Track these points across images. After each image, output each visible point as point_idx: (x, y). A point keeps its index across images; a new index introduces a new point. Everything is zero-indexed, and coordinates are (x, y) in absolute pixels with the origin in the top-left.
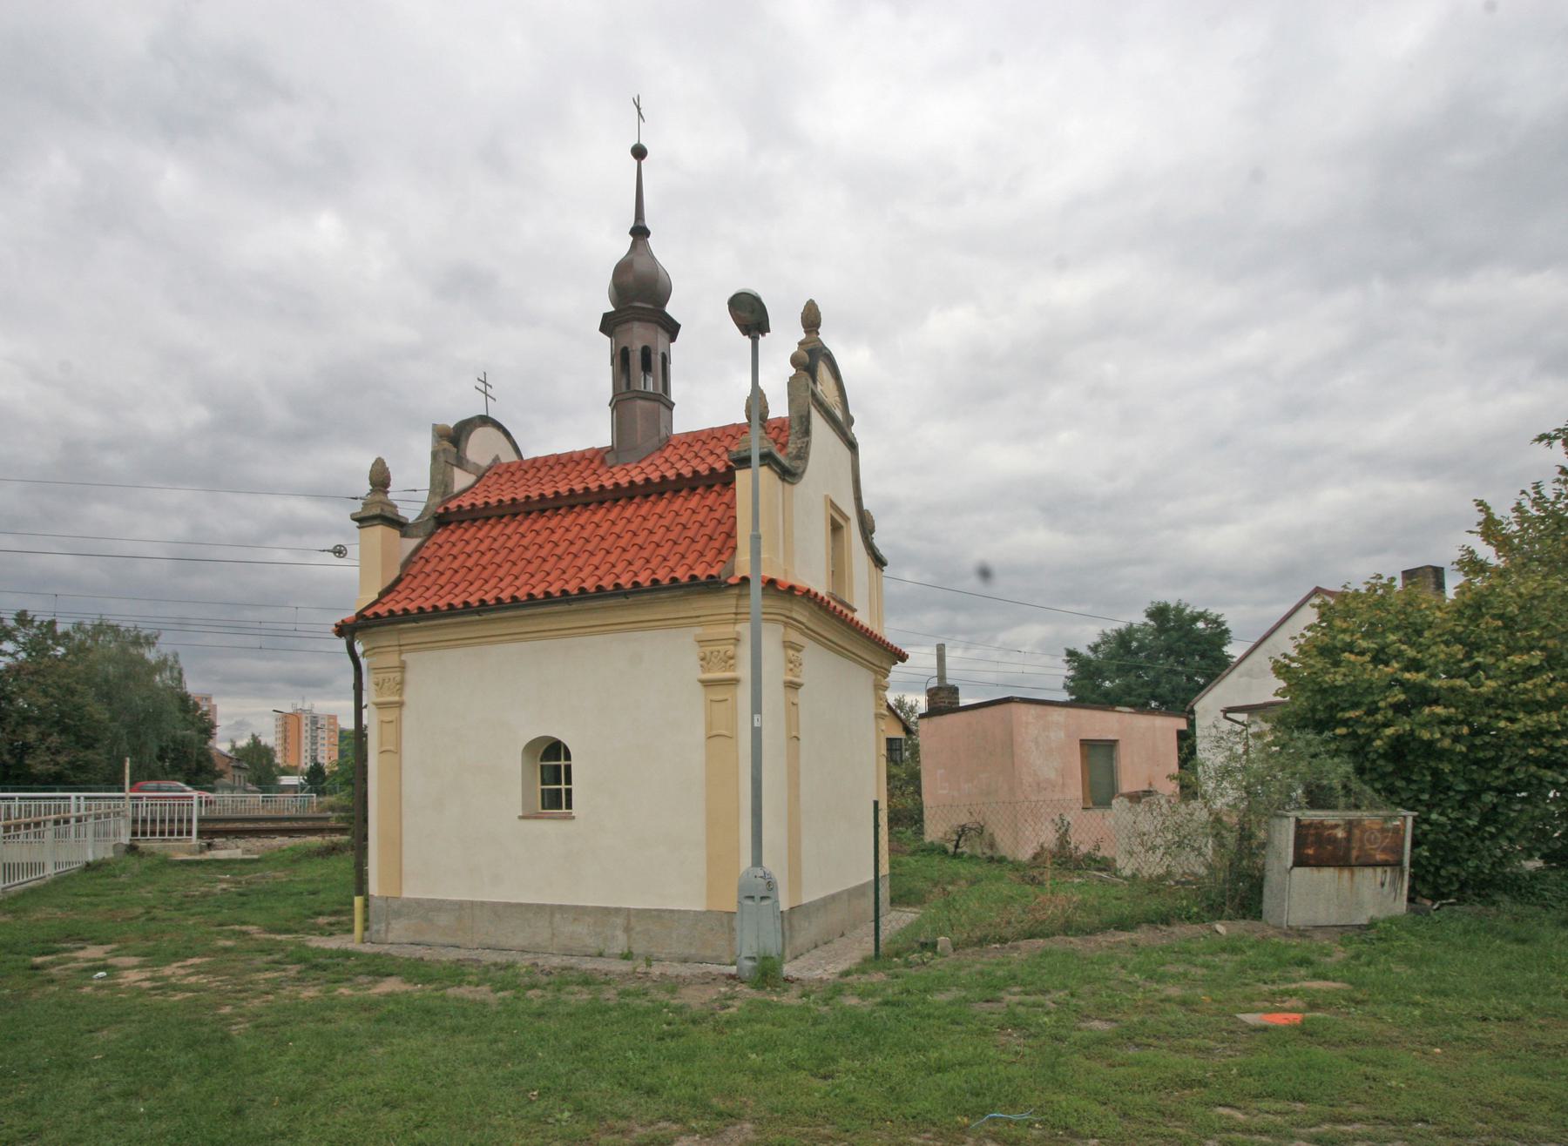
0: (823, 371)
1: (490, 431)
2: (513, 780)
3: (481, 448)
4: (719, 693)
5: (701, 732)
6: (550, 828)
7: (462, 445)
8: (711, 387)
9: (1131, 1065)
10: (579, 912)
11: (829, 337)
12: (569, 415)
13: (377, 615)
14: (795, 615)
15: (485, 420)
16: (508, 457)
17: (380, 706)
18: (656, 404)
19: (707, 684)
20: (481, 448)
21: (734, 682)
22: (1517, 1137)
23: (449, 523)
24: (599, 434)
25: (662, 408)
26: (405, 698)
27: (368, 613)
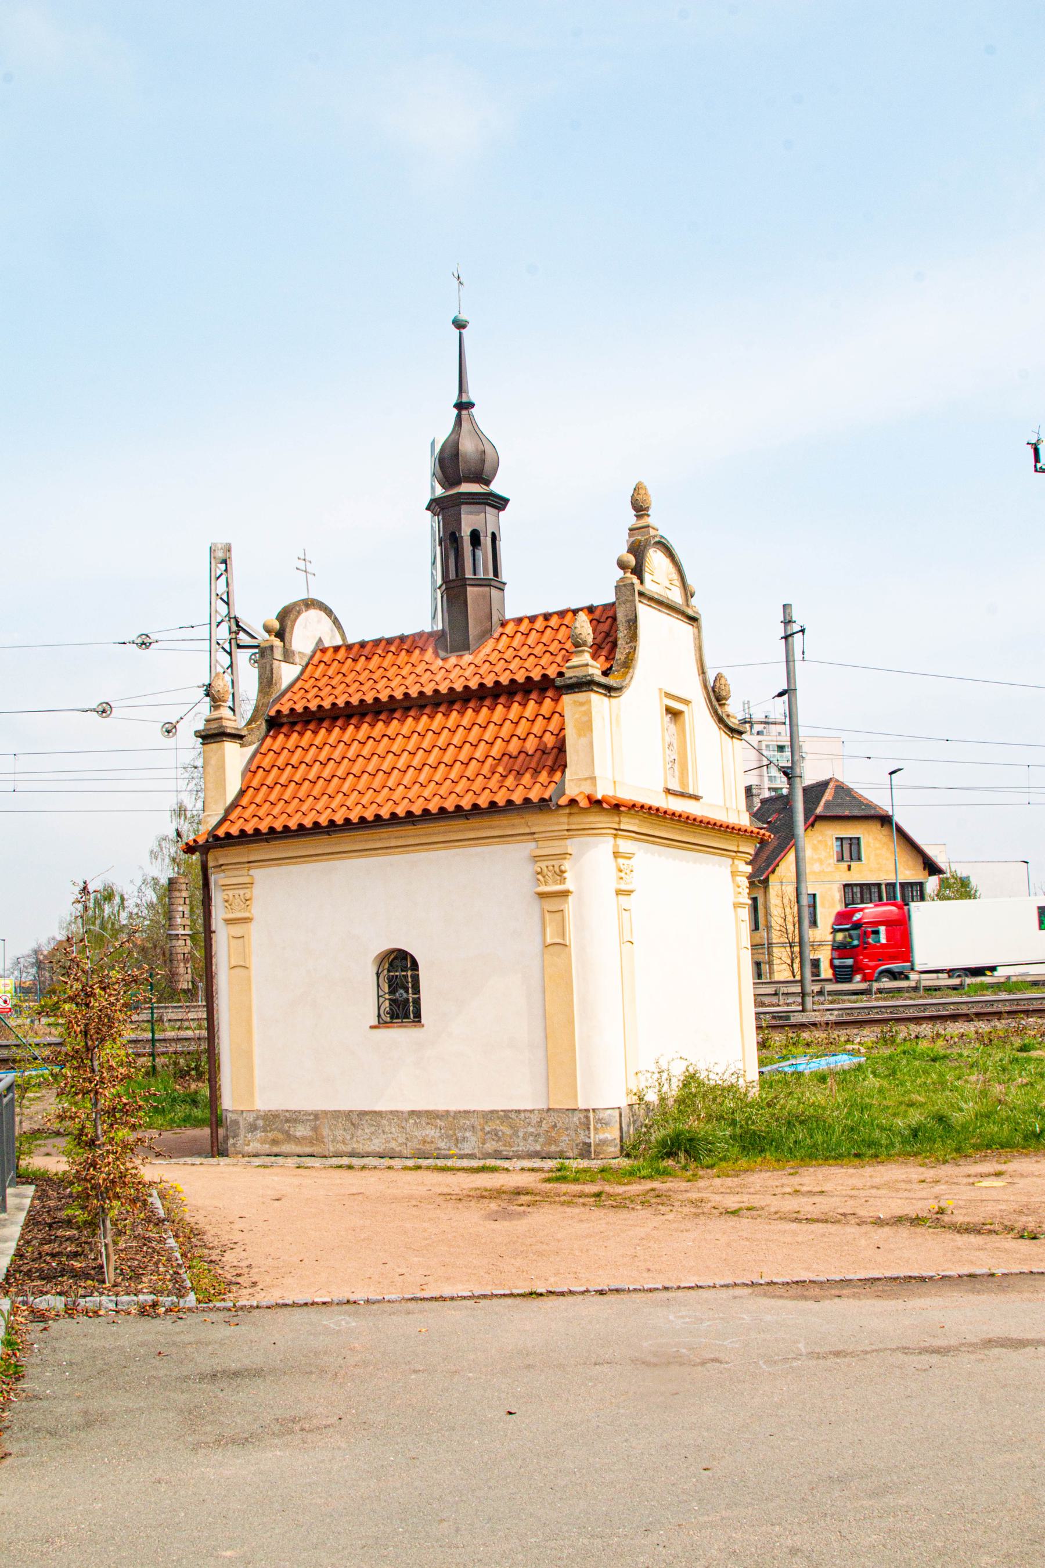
0: (655, 559)
1: (314, 614)
2: (366, 995)
3: (309, 633)
4: (552, 905)
5: (536, 946)
6: (400, 1035)
7: (287, 635)
8: (548, 568)
9: (536, 1194)
10: (431, 1116)
11: (659, 521)
12: (393, 594)
13: (228, 835)
14: (622, 827)
15: (310, 604)
16: (332, 639)
17: (228, 922)
18: (487, 589)
19: (542, 896)
20: (309, 633)
21: (565, 894)
22: (211, 1309)
23: (282, 725)
24: (417, 611)
25: (494, 591)
26: (256, 910)
27: (221, 833)
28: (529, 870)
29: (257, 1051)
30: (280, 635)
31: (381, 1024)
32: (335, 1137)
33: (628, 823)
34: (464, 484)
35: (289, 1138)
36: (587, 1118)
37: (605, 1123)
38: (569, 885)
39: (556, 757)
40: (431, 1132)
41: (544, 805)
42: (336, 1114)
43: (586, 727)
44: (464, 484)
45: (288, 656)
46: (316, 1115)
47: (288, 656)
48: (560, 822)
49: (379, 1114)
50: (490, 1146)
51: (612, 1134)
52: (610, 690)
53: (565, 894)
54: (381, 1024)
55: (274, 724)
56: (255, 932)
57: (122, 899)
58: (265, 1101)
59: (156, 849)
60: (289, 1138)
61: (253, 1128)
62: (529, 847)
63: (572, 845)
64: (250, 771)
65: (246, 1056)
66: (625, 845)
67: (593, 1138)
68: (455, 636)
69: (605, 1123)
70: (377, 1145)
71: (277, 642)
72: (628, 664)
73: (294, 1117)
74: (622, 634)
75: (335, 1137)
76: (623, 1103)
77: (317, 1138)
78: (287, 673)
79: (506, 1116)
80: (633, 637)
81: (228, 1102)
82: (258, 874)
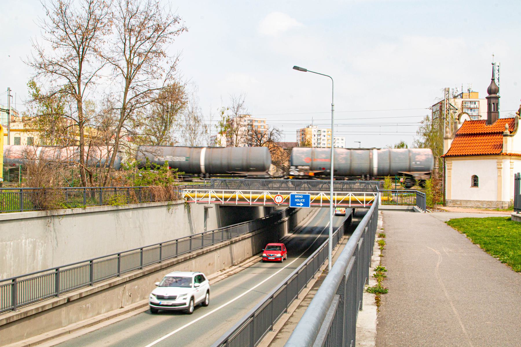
2: (470, 182)
6: (475, 189)
10: (479, 201)
21: (501, 168)
26: (452, 168)
28: (496, 164)
29: (452, 190)
30: (458, 119)
31: (472, 186)
32: (464, 204)
33: (512, 157)
34: (493, 93)
35: (456, 204)
36: (503, 203)
37: (506, 203)
38: (502, 167)
39: (501, 146)
40: (479, 204)
41: (498, 154)
42: (464, 201)
43: (506, 142)
44: (493, 93)
45: (459, 123)
46: (461, 201)
47: (459, 123)
48: (501, 157)
49: (471, 201)
50: (488, 206)
51: (507, 205)
52: (511, 136)
53: (501, 168)
54: (472, 186)
55: (457, 136)
56: (452, 171)
57: (407, 146)
58: (452, 198)
59: (419, 131)
60: (456, 204)
61: (450, 202)
62: (496, 160)
63: (503, 161)
64: (452, 144)
65: (450, 190)
66: (512, 161)
67: (504, 206)
68: (489, 122)
69: (506, 203)
70: (470, 206)
71: (457, 121)
72: (516, 131)
73: (457, 201)
74: (516, 125)
75: (464, 204)
76: (509, 201)
77: (461, 204)
78: (459, 126)
79: (491, 202)
80: (517, 126)
81: (446, 198)
82: (453, 162)
